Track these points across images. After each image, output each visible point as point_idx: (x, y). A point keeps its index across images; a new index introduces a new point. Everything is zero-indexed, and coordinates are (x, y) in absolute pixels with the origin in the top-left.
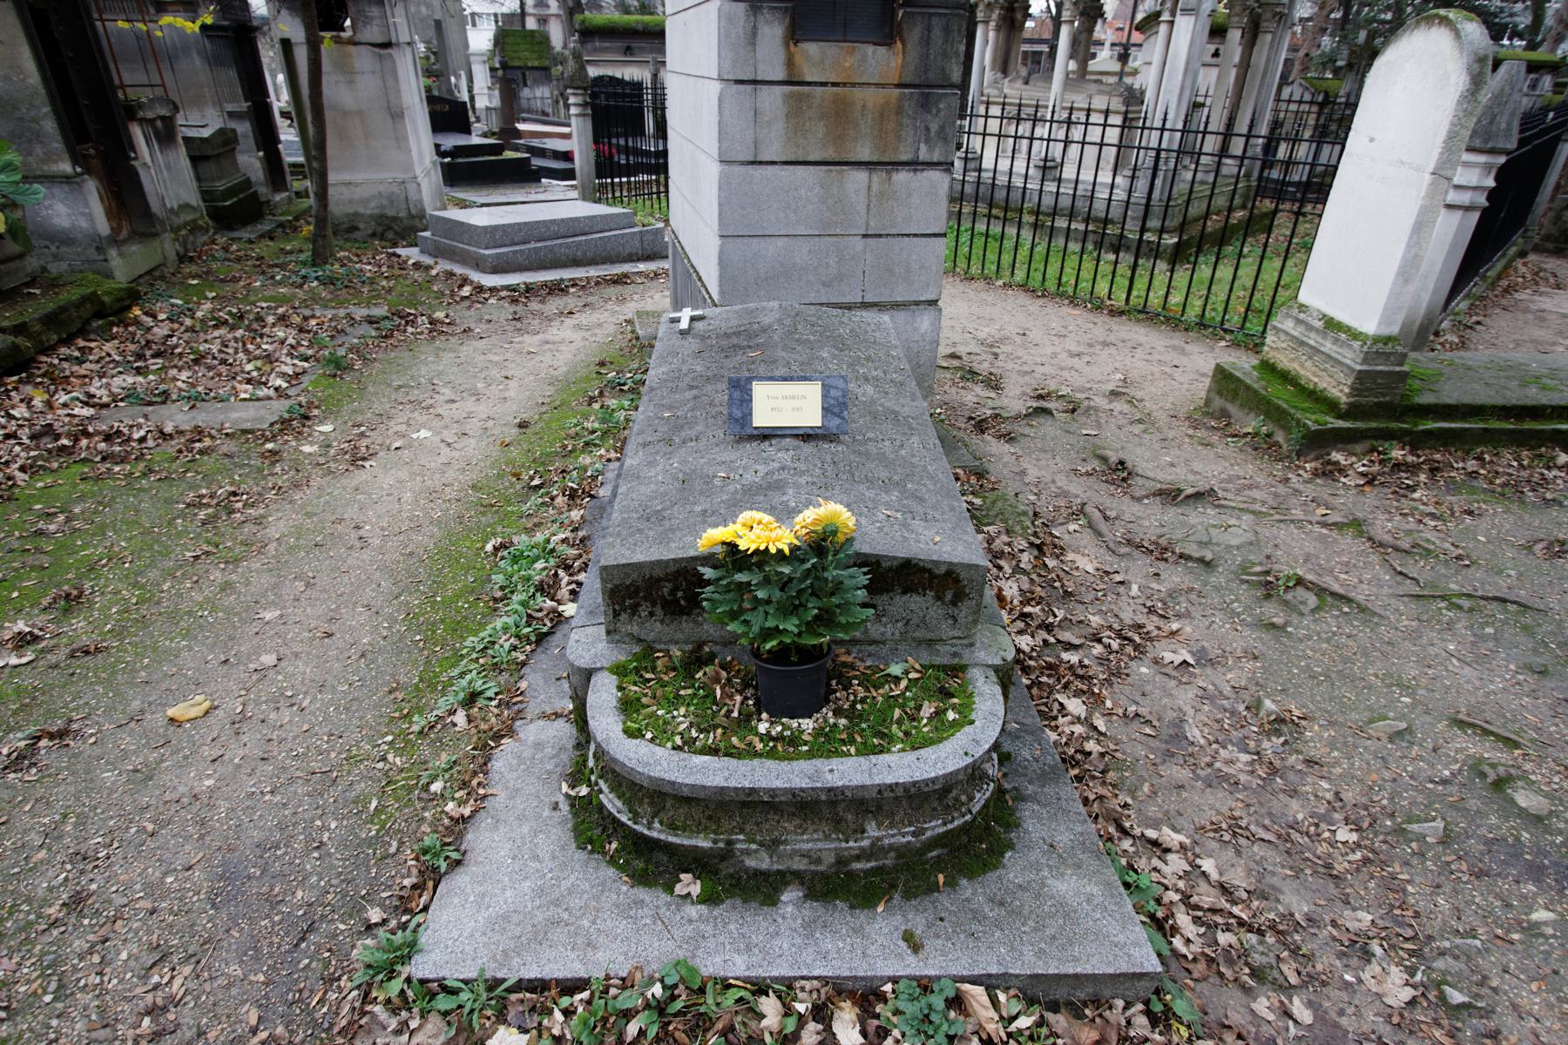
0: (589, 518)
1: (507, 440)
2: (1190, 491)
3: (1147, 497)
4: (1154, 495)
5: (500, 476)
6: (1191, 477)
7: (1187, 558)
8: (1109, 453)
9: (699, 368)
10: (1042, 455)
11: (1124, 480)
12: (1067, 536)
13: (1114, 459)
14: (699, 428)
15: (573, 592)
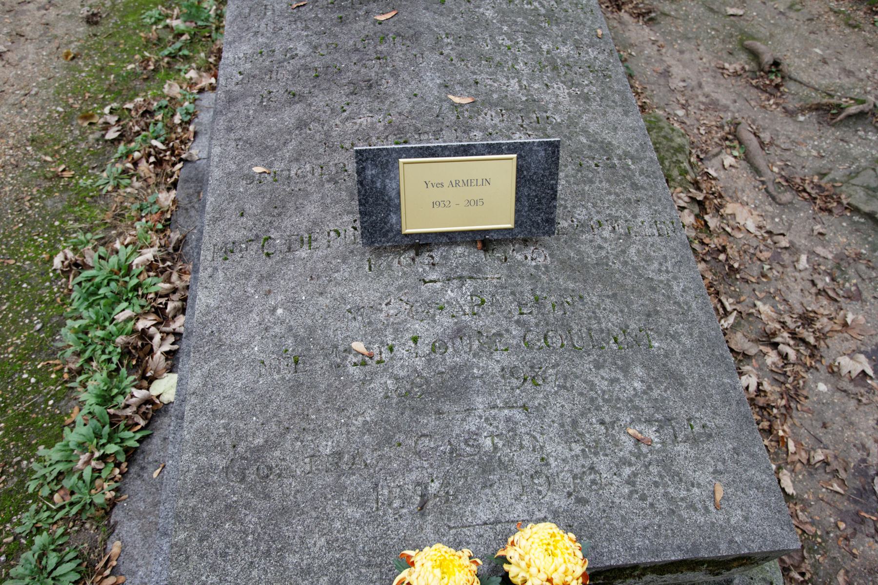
0: (184, 203)
1: (73, 49)
2: (853, 109)
3: (802, 110)
4: (811, 109)
5: (67, 118)
6: (846, 81)
7: (855, 210)
8: (759, 46)
9: (301, 49)
10: (686, 46)
11: (777, 86)
12: (722, 175)
13: (767, 59)
14: (312, 209)
15: (170, 355)
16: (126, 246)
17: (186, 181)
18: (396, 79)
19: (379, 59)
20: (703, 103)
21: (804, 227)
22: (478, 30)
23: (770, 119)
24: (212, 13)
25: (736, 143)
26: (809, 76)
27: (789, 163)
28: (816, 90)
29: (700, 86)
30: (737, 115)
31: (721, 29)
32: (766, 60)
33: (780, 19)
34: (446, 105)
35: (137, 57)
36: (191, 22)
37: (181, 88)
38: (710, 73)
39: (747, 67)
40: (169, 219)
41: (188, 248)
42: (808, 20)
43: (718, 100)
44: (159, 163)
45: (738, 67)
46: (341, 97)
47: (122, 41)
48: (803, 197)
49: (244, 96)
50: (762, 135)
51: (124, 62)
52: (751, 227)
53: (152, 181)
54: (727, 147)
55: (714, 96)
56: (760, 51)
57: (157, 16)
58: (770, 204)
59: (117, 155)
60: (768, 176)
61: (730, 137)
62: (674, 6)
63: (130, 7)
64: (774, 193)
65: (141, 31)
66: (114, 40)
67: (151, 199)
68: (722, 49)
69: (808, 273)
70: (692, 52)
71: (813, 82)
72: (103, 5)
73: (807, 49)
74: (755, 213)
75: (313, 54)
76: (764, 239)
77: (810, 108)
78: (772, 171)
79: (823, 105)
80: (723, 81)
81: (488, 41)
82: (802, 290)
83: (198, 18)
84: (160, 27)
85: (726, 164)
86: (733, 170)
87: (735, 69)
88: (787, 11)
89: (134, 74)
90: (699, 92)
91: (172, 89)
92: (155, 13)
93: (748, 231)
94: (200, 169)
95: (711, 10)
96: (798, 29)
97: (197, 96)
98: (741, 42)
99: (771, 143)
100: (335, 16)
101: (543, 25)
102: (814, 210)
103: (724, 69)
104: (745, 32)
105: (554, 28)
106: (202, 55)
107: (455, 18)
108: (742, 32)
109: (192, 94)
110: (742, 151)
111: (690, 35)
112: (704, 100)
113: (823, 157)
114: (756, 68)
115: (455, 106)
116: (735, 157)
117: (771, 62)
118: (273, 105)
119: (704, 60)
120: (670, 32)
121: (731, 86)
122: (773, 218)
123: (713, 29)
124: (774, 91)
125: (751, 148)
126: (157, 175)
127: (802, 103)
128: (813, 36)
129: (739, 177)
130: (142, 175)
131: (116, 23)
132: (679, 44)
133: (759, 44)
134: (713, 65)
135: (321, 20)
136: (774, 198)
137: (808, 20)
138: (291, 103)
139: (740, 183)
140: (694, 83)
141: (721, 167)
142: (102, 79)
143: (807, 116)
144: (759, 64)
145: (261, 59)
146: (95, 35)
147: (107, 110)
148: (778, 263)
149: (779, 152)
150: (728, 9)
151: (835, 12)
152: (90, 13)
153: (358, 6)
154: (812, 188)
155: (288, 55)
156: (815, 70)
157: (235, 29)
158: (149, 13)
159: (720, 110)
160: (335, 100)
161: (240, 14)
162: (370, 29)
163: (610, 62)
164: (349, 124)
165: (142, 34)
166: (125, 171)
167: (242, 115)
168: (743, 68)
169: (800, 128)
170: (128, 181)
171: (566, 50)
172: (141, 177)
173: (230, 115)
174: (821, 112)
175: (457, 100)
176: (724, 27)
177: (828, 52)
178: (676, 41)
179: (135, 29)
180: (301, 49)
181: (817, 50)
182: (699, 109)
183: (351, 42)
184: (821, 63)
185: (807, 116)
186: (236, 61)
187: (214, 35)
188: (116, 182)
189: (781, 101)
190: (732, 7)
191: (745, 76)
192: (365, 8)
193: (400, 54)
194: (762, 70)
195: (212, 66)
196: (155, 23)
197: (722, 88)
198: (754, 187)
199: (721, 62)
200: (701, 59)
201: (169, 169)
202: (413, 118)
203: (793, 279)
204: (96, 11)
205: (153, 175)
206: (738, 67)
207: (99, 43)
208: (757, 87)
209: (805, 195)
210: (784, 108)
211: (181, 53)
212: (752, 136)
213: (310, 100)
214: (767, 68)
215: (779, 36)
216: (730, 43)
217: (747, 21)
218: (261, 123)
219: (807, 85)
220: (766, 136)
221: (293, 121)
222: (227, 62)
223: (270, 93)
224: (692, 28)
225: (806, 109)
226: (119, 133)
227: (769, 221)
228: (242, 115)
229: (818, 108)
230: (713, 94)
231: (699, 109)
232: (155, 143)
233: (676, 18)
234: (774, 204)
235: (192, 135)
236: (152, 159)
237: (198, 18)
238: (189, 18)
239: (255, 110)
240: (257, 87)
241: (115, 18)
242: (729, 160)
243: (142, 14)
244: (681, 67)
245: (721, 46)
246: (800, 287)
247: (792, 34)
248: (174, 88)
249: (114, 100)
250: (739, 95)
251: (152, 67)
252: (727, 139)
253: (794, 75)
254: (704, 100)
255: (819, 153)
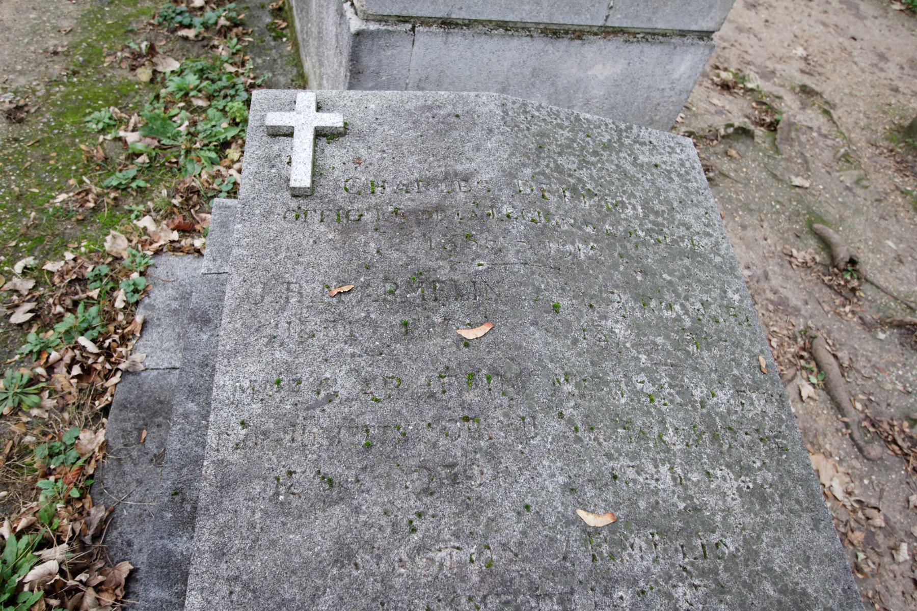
4: (892, 325)
8: (830, 232)
9: (345, 385)
11: (853, 290)
13: (843, 254)
16: (19, 536)
17: (123, 407)
18: (495, 468)
19: (466, 419)
20: (772, 302)
21: (897, 494)
22: (608, 365)
23: (847, 332)
24: (183, 129)
25: (813, 365)
26: (886, 279)
27: (873, 398)
28: (896, 299)
29: (766, 277)
30: (810, 323)
31: (787, 204)
32: (841, 256)
33: (847, 196)
34: (575, 532)
35: (72, 182)
36: (153, 138)
37: (130, 241)
38: (777, 260)
39: (818, 259)
40: (91, 477)
41: (115, 533)
42: (877, 200)
43: (787, 299)
44: (87, 371)
45: (808, 258)
46: (407, 499)
47: (54, 154)
48: (893, 451)
49: (247, 476)
50: (839, 354)
51: (52, 189)
52: (839, 493)
53: (71, 400)
54: (803, 368)
55: (784, 292)
56: (833, 240)
57: (107, 120)
58: (857, 458)
59: (26, 349)
60: (852, 417)
61: (805, 354)
62: (733, 165)
63: (71, 100)
64: (861, 443)
65: (81, 142)
66: (42, 151)
67: (68, 439)
68: (788, 230)
69: (908, 566)
70: (755, 230)
71: (891, 288)
72: (34, 92)
73: (880, 241)
74: (841, 469)
75: (362, 397)
76: (854, 511)
77: (891, 323)
78: (855, 408)
79: (907, 324)
80: (790, 273)
81: (623, 385)
82: (903, 593)
83: (164, 134)
84: (109, 137)
85: (804, 394)
86: (812, 403)
87: (804, 258)
88: (854, 186)
89: (65, 213)
90: (765, 285)
91: (116, 242)
92: (104, 114)
93: (835, 497)
94: (145, 387)
95: (775, 176)
96: (868, 211)
97: (151, 262)
98: (810, 224)
99: (851, 367)
100: (396, 319)
101: (690, 348)
102: (906, 470)
103: (791, 256)
104: (813, 212)
105: (705, 354)
106: (165, 192)
107: (575, 342)
108: (811, 212)
109: (144, 256)
110: (820, 378)
111: (753, 206)
112: (770, 295)
113: (909, 393)
114: (828, 262)
115: (590, 533)
116: (813, 385)
117: (848, 260)
118: (296, 502)
119: (769, 241)
120: (730, 200)
121: (800, 280)
122: (861, 480)
123: (778, 202)
124: (850, 296)
125: (831, 376)
126: (81, 390)
127: (881, 314)
128: (883, 223)
129: (818, 415)
130: (59, 387)
131: (47, 124)
132: (741, 216)
133: (831, 231)
134: (779, 249)
135: (375, 325)
136: (860, 450)
137: (877, 200)
138: (328, 503)
139: (821, 423)
140: (759, 272)
141: (797, 396)
142: (17, 214)
143: (888, 333)
144: (832, 258)
145: (278, 397)
146: (16, 140)
147: (18, 267)
148: (872, 549)
149: (860, 381)
150: (793, 178)
151: (902, 192)
152: (13, 106)
153: (432, 304)
154: (904, 440)
155: (323, 394)
156: (891, 271)
157: (238, 326)
158: (96, 114)
159: (791, 314)
160: (398, 503)
161: (248, 295)
162: (451, 357)
163: (781, 420)
164: (421, 561)
165: (83, 147)
166: (34, 380)
167: (243, 521)
168: (814, 259)
169: (881, 348)
170: (35, 399)
171: (724, 399)
172: (56, 391)
173: (222, 519)
174: (903, 331)
175: (591, 520)
176: (790, 201)
177: (901, 246)
178: (737, 212)
179: (74, 136)
180: (345, 385)
181: (890, 243)
182: (767, 310)
183: (423, 380)
184: (896, 262)
185: (888, 333)
186: (237, 395)
187: (182, 160)
188: (17, 400)
189: (858, 309)
190: (797, 175)
191: (816, 270)
192: (443, 309)
193: (499, 413)
194: (836, 266)
195: (175, 210)
196: (103, 131)
197: (791, 282)
198: (837, 430)
199: (788, 246)
200: (766, 240)
201: (99, 384)
202: (526, 560)
203: (892, 575)
204: (22, 103)
205: (74, 390)
206: (808, 258)
207: (20, 153)
208: (830, 287)
209: (896, 448)
210: (861, 318)
211: (134, 185)
212: (832, 359)
213: (358, 499)
214: (842, 265)
215: (849, 220)
216: (797, 222)
217: (814, 195)
218: (273, 543)
219: (885, 291)
220: (843, 355)
221: (329, 544)
222: (223, 396)
223: (290, 473)
224: (754, 197)
225: (887, 323)
226: (31, 315)
227: (857, 483)
228: (243, 521)
229: (900, 325)
230: (781, 290)
231: (767, 310)
232: (83, 341)
233: (737, 182)
234: (861, 457)
235: (139, 328)
236: (76, 370)
237: (164, 134)
238: (150, 131)
239: (265, 512)
240: (270, 459)
241: (48, 116)
242: (807, 391)
243: (86, 115)
244: (744, 247)
245: (786, 225)
246: (901, 588)
247: (863, 219)
248: (119, 241)
249: (31, 252)
250: (810, 293)
251: (92, 205)
252: (802, 357)
253: (870, 276)
254: (770, 295)
255: (905, 387)
